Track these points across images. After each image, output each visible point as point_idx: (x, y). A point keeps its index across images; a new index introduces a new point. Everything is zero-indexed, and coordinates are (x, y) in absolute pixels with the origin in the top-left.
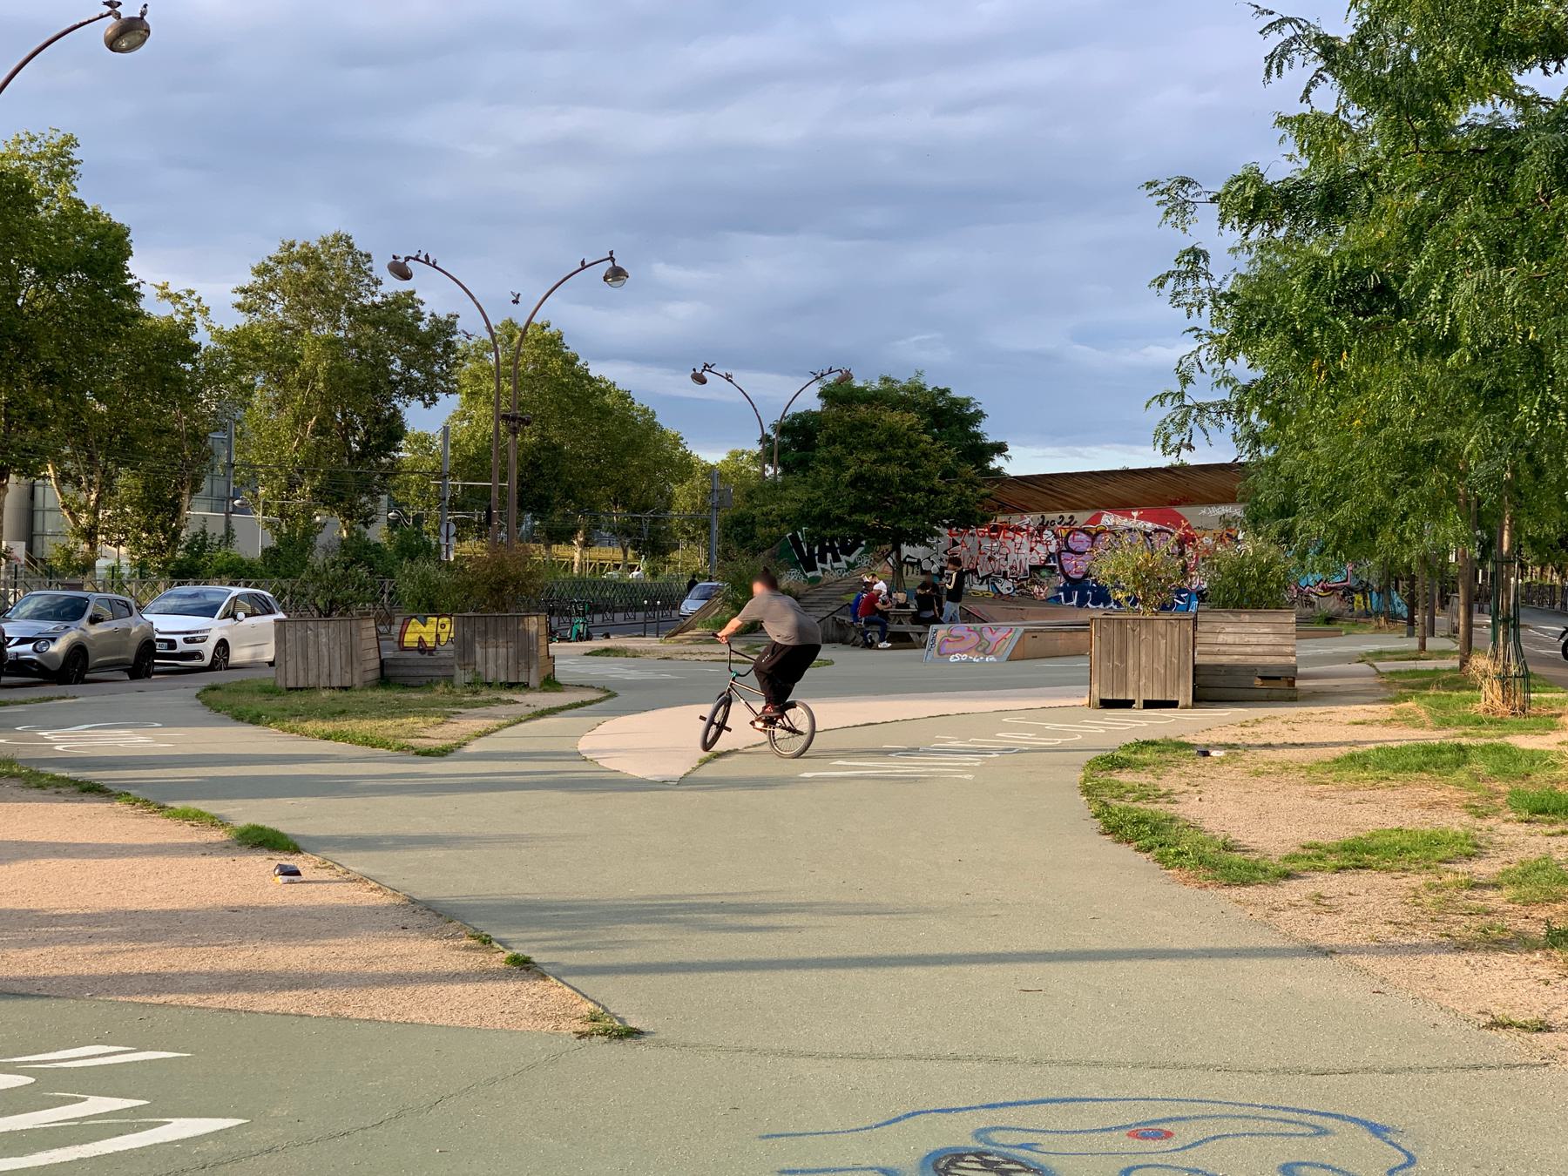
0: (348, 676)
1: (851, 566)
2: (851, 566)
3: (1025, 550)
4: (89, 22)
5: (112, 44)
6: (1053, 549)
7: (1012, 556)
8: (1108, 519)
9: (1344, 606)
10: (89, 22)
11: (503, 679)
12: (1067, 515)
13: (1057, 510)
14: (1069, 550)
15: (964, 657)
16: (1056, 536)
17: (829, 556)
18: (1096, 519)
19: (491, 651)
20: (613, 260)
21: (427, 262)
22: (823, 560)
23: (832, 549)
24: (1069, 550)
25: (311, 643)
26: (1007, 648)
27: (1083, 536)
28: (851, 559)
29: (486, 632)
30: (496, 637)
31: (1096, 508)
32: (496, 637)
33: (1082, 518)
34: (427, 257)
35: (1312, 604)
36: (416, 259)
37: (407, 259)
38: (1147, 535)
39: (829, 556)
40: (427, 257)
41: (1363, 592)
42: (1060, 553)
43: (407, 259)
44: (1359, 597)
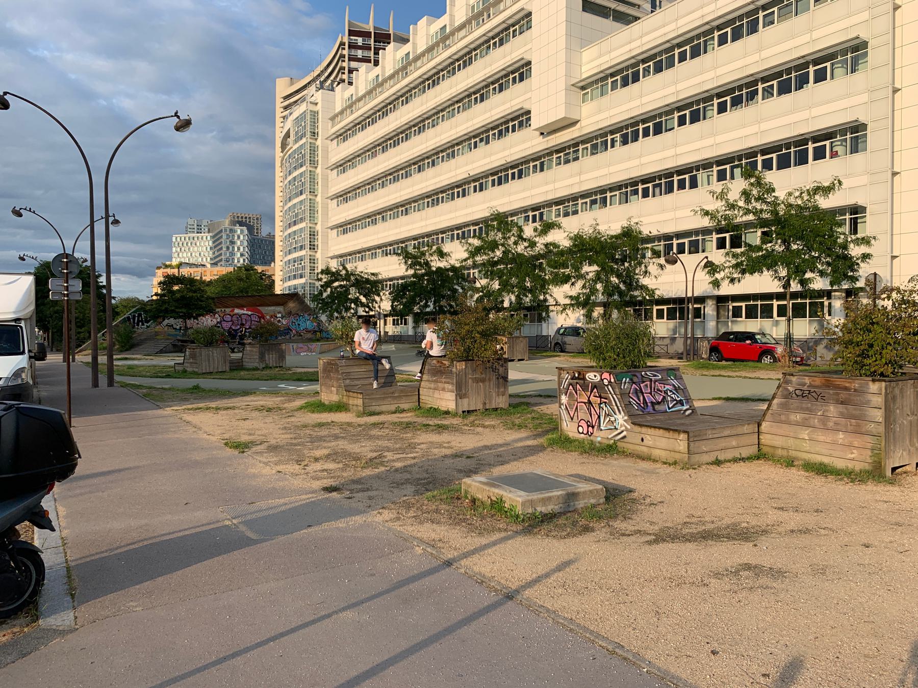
0: (224, 367)
1: (148, 327)
2: (148, 327)
3: (209, 321)
4: (163, 118)
5: (178, 128)
6: (219, 320)
7: (205, 323)
8: (237, 311)
9: (313, 336)
10: (163, 118)
11: (275, 365)
12: (223, 310)
13: (220, 308)
14: (224, 321)
15: (305, 353)
16: (220, 316)
17: (140, 323)
18: (233, 311)
19: (271, 356)
20: (114, 217)
21: (30, 211)
22: (138, 325)
23: (142, 321)
24: (224, 321)
25: (211, 356)
26: (318, 350)
27: (229, 316)
28: (148, 325)
29: (269, 350)
30: (272, 351)
31: (232, 307)
32: (272, 351)
33: (228, 310)
34: (30, 209)
35: (301, 336)
36: (25, 209)
37: (21, 209)
38: (250, 316)
39: (140, 323)
40: (30, 209)
41: (320, 332)
42: (221, 321)
43: (21, 209)
44: (318, 333)
